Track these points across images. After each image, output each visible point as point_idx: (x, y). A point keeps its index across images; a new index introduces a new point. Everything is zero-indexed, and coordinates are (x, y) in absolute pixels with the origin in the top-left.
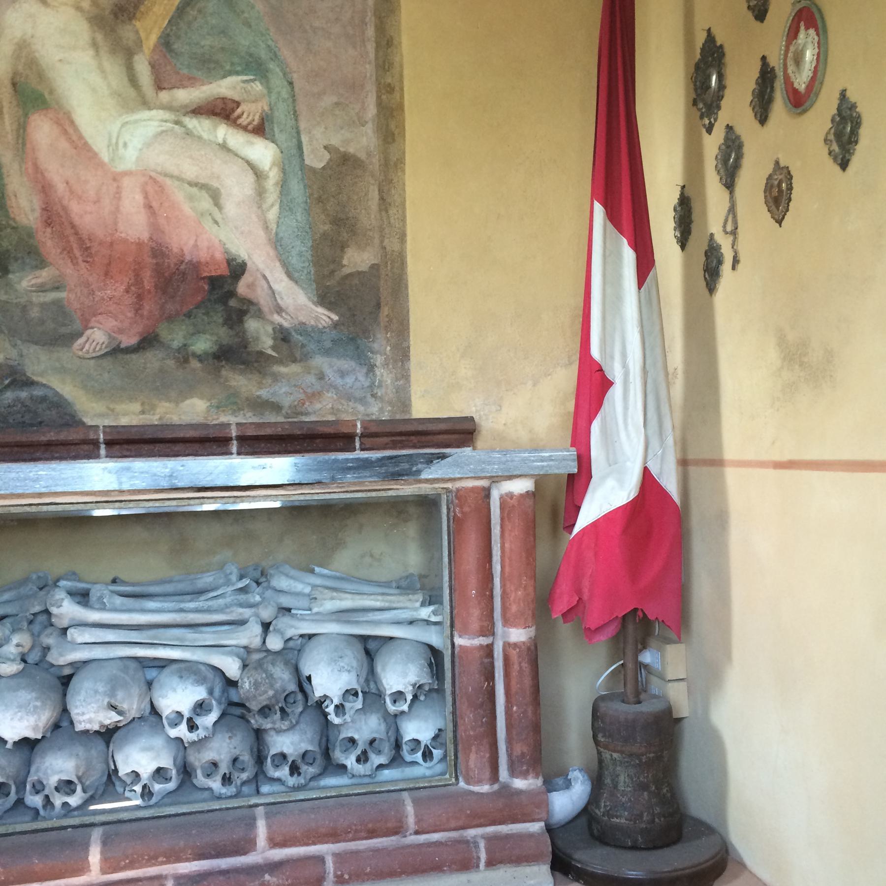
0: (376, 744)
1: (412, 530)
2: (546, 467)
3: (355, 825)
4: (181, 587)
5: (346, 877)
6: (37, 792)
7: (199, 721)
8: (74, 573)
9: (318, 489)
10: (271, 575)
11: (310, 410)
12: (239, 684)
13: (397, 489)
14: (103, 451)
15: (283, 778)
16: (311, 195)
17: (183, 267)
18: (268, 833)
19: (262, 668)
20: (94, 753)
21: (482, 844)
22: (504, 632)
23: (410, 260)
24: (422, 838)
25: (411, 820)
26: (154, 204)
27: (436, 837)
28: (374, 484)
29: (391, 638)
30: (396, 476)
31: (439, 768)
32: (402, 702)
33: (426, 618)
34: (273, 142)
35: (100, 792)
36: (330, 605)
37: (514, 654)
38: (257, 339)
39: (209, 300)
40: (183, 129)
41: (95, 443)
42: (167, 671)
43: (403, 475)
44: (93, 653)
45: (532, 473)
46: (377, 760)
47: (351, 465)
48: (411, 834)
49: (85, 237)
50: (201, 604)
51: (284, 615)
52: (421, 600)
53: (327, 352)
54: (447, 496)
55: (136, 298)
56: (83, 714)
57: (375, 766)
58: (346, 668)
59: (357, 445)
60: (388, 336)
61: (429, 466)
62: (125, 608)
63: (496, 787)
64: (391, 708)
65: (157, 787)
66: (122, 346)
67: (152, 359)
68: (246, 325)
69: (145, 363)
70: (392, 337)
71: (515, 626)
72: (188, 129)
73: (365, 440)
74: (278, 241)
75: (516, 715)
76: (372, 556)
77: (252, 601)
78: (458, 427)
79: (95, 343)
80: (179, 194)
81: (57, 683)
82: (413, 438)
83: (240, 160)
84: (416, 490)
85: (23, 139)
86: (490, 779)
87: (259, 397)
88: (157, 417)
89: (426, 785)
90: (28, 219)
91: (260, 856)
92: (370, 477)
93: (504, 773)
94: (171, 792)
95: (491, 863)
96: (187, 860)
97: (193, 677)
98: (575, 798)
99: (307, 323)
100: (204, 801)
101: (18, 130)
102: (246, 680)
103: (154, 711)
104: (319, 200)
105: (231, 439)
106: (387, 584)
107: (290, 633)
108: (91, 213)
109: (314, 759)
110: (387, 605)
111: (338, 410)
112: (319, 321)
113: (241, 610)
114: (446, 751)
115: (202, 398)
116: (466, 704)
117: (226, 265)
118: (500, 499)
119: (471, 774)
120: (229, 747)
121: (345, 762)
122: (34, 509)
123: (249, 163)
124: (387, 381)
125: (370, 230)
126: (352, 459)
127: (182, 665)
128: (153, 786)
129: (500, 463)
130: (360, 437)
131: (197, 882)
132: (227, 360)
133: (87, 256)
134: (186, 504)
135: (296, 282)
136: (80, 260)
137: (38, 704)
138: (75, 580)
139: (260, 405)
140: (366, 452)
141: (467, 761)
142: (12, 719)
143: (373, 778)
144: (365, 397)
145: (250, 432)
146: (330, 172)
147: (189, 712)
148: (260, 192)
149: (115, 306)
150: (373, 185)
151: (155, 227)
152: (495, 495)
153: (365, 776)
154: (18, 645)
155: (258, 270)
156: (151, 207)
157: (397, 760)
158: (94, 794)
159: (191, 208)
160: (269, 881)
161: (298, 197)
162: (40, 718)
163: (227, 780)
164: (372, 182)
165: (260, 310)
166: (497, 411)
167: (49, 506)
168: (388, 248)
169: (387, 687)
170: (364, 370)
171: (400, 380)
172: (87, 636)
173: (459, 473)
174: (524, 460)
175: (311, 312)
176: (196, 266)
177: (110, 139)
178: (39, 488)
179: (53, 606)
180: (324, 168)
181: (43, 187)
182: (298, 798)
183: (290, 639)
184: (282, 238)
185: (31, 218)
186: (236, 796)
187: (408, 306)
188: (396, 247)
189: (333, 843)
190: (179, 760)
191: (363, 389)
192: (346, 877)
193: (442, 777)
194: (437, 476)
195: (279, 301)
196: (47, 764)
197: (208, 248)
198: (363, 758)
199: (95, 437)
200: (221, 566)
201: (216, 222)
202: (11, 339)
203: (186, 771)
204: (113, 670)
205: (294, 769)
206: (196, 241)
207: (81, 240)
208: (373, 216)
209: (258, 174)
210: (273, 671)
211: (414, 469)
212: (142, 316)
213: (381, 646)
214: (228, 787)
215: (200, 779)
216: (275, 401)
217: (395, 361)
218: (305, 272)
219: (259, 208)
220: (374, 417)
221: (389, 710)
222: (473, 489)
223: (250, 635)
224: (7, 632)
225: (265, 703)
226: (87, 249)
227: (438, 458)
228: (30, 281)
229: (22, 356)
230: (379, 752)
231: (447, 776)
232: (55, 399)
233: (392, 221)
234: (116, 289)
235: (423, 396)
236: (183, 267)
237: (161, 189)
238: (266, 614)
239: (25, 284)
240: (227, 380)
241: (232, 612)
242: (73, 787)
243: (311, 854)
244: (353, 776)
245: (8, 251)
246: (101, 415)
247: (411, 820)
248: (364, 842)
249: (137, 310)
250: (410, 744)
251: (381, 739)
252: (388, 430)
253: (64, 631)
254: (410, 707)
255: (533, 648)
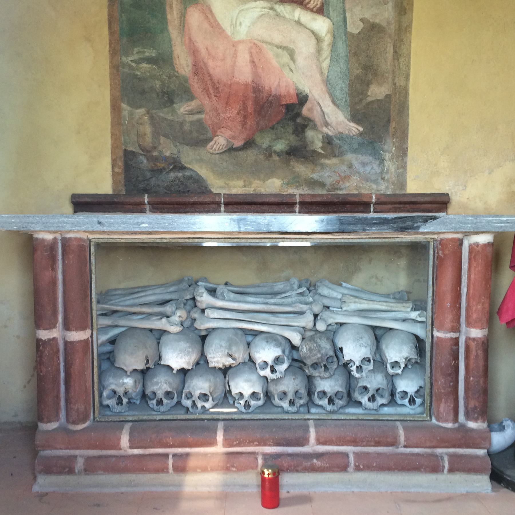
0: (380, 391)
1: (403, 263)
2: (504, 227)
3: (368, 438)
4: (265, 290)
5: (361, 467)
6: (188, 398)
7: (277, 368)
8: (206, 278)
9: (353, 235)
10: (318, 286)
11: (342, 187)
12: (300, 349)
13: (402, 238)
14: (223, 209)
15: (324, 406)
16: (350, 51)
17: (270, 99)
18: (316, 435)
19: (314, 340)
20: (218, 379)
21: (446, 459)
22: (467, 330)
23: (411, 92)
24: (408, 450)
25: (402, 439)
26: (256, 60)
27: (416, 450)
28: (388, 234)
29: (391, 329)
30: (403, 230)
31: (419, 410)
32: (398, 368)
33: (414, 318)
34: (328, 18)
35: (220, 402)
36: (354, 306)
37: (473, 345)
38: (313, 142)
39: (285, 119)
40: (274, 12)
41: (219, 204)
42: (258, 338)
43: (408, 229)
44: (219, 324)
45: (494, 230)
46: (380, 401)
47: (375, 221)
48: (402, 447)
49: (216, 81)
50: (278, 300)
51: (326, 310)
52: (411, 307)
53: (355, 151)
54: (434, 244)
55: (243, 118)
56: (214, 358)
57: (379, 404)
58: (364, 344)
59: (372, 209)
60: (394, 140)
61: (425, 224)
62: (235, 300)
63: (456, 425)
64: (391, 371)
65: (253, 403)
66: (234, 147)
67: (251, 155)
68: (307, 134)
69: (247, 157)
70: (396, 141)
71: (475, 327)
72: (278, 12)
73: (376, 206)
74: (328, 81)
75: (472, 383)
76: (377, 278)
77: (308, 301)
78: (439, 199)
79: (219, 145)
80: (270, 53)
81: (199, 339)
82: (407, 206)
83: (308, 30)
84: (414, 239)
85: (184, 23)
86: (453, 420)
87: (312, 178)
88: (253, 189)
89: (411, 419)
90: (186, 72)
91: (311, 449)
92: (387, 229)
93: (461, 417)
94: (260, 406)
95: (451, 470)
96: (270, 445)
97: (274, 342)
98: (507, 437)
99: (344, 132)
100: (278, 413)
101: (181, 18)
102: (304, 346)
103: (250, 359)
104: (355, 54)
105: (296, 203)
106: (387, 296)
107: (330, 321)
108: (220, 67)
109: (342, 396)
110: (389, 308)
111: (360, 187)
112: (351, 132)
113: (301, 306)
114: (424, 400)
115: (278, 179)
116: (440, 373)
117: (296, 96)
118: (469, 246)
119: (441, 416)
120: (293, 384)
121: (361, 400)
122: (191, 241)
123: (313, 32)
124: (391, 169)
125: (386, 73)
126: (376, 218)
127: (268, 335)
128: (251, 402)
129: (472, 223)
130: (374, 205)
131: (275, 459)
132: (295, 155)
133: (217, 93)
134: (274, 241)
135: (338, 107)
136: (213, 96)
137: (190, 350)
138: (206, 282)
139: (313, 183)
140: (377, 214)
141: (439, 408)
142: (176, 357)
143: (377, 411)
144: (377, 179)
145: (308, 200)
146: (362, 36)
147: (272, 362)
148: (319, 51)
149: (231, 122)
150: (390, 43)
151: (256, 74)
152: (466, 244)
153: (373, 409)
154: (180, 317)
155: (315, 100)
156: (254, 62)
157: (392, 402)
158: (218, 403)
159: (277, 62)
160: (316, 463)
161: (342, 53)
162: (191, 358)
163: (292, 403)
164: (390, 41)
165: (315, 125)
166: (463, 189)
167: (199, 239)
168: (398, 84)
169: (388, 358)
170: (378, 162)
171: (400, 169)
172: (216, 314)
173: (444, 229)
174: (488, 222)
175: (346, 126)
176: (278, 98)
177: (232, 21)
178: (196, 229)
179: (198, 296)
180: (359, 33)
181: (194, 52)
182: (333, 418)
183: (330, 325)
184: (331, 79)
185: (187, 71)
186: (297, 412)
187: (408, 122)
188: (403, 83)
189: (354, 446)
190: (265, 389)
191: (376, 174)
192: (361, 467)
193: (421, 415)
194: (430, 230)
195: (327, 119)
196: (194, 384)
197: (286, 86)
198: (372, 399)
199: (219, 200)
200: (288, 280)
201: (292, 71)
202: (174, 142)
203: (268, 395)
204: (230, 334)
205: (331, 401)
206: (279, 82)
207: (214, 84)
208: (389, 64)
209: (318, 39)
210: (320, 343)
211: (415, 225)
212: (246, 129)
213: (385, 333)
214: (292, 407)
215: (276, 401)
216: (321, 181)
217: (398, 157)
218: (344, 100)
219: (317, 60)
220: (382, 192)
221: (389, 372)
222: (453, 240)
223: (307, 321)
224: (174, 309)
225: (315, 361)
226: (217, 88)
227: (431, 219)
228: (184, 108)
229: (179, 152)
230: (382, 396)
231: (425, 415)
232: (197, 178)
233: (401, 66)
234: (232, 112)
235: (415, 179)
236: (270, 99)
237: (260, 51)
238: (317, 309)
239: (182, 110)
240: (293, 167)
241: (296, 306)
242: (207, 398)
243: (341, 451)
244: (366, 409)
245: (174, 90)
246: (221, 187)
247: (402, 439)
248: (372, 448)
249: (243, 125)
250: (400, 393)
251: (383, 389)
252: (393, 200)
253: (203, 311)
254: (402, 371)
255: (486, 342)
